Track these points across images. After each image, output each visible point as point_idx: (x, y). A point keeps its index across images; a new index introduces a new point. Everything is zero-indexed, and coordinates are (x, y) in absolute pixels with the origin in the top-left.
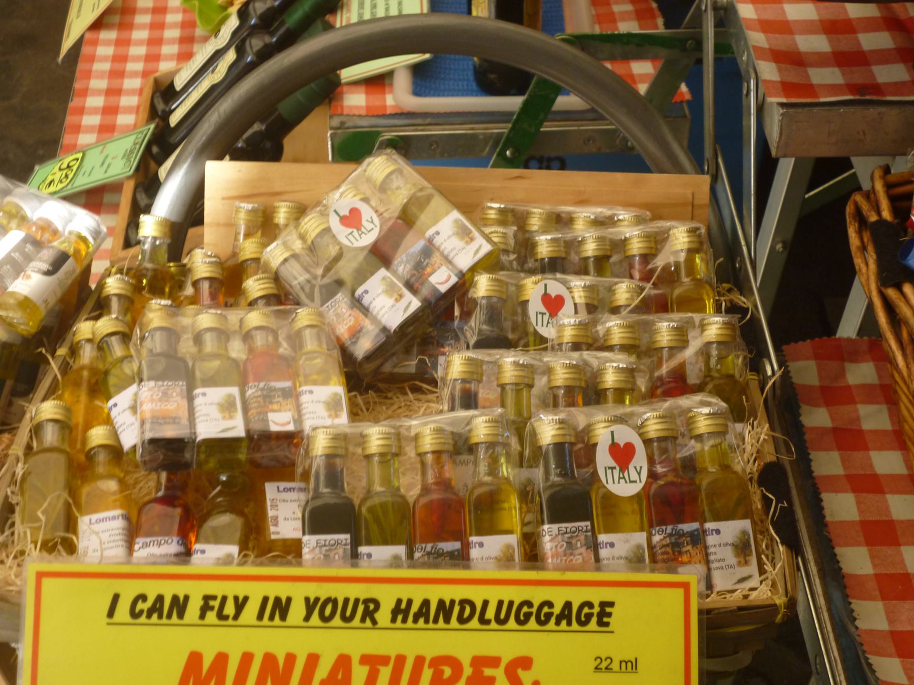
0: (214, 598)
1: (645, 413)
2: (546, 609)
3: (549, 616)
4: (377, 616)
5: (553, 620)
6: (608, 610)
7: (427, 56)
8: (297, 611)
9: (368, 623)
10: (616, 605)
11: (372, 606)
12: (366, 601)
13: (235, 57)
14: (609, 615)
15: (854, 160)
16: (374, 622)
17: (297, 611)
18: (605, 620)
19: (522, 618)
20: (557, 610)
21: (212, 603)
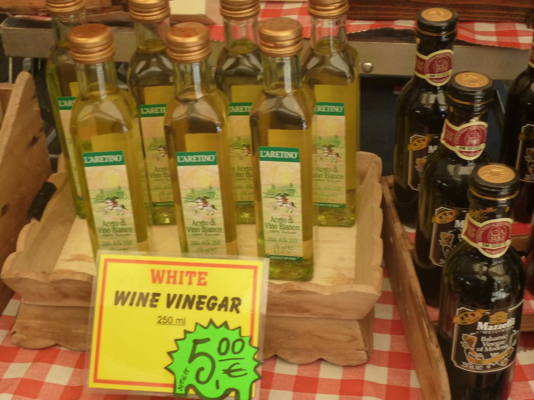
0: (205, 297)
1: (475, 197)
2: (213, 301)
3: (214, 305)
4: (240, 308)
5: (217, 307)
6: (157, 298)
7: (396, 146)
8: (163, 300)
9: (234, 311)
10: (169, 293)
11: (237, 302)
12: (234, 299)
13: (379, 160)
14: (157, 301)
15: (50, 180)
16: (238, 312)
17: (163, 300)
18: (155, 303)
19: (211, 306)
20: (219, 302)
21: (203, 300)
